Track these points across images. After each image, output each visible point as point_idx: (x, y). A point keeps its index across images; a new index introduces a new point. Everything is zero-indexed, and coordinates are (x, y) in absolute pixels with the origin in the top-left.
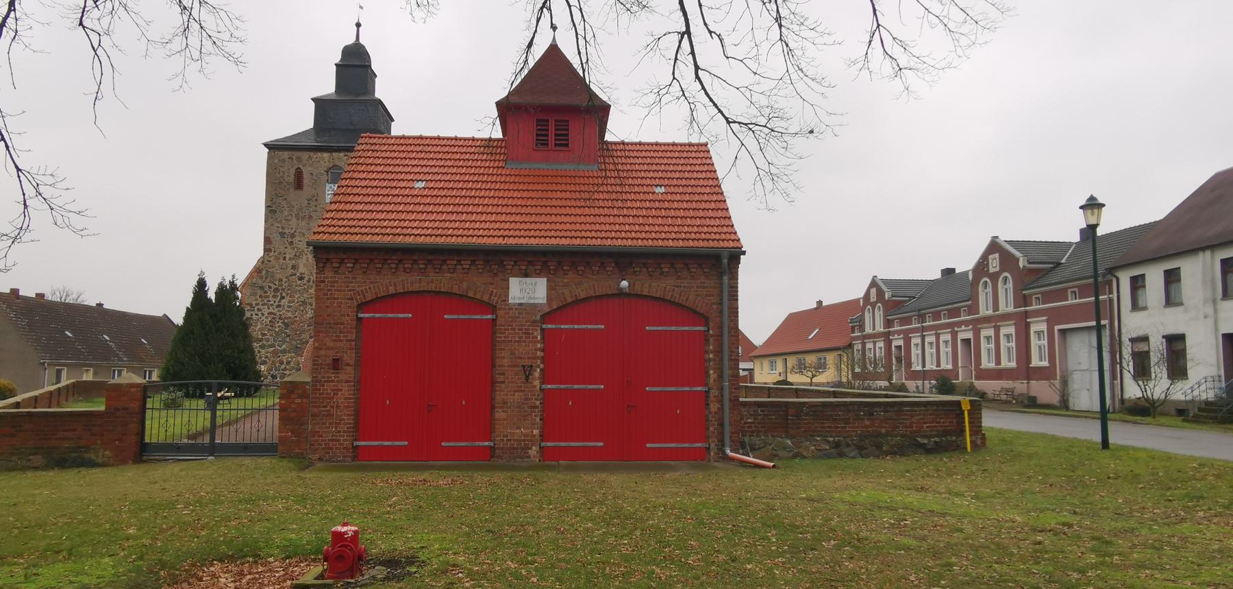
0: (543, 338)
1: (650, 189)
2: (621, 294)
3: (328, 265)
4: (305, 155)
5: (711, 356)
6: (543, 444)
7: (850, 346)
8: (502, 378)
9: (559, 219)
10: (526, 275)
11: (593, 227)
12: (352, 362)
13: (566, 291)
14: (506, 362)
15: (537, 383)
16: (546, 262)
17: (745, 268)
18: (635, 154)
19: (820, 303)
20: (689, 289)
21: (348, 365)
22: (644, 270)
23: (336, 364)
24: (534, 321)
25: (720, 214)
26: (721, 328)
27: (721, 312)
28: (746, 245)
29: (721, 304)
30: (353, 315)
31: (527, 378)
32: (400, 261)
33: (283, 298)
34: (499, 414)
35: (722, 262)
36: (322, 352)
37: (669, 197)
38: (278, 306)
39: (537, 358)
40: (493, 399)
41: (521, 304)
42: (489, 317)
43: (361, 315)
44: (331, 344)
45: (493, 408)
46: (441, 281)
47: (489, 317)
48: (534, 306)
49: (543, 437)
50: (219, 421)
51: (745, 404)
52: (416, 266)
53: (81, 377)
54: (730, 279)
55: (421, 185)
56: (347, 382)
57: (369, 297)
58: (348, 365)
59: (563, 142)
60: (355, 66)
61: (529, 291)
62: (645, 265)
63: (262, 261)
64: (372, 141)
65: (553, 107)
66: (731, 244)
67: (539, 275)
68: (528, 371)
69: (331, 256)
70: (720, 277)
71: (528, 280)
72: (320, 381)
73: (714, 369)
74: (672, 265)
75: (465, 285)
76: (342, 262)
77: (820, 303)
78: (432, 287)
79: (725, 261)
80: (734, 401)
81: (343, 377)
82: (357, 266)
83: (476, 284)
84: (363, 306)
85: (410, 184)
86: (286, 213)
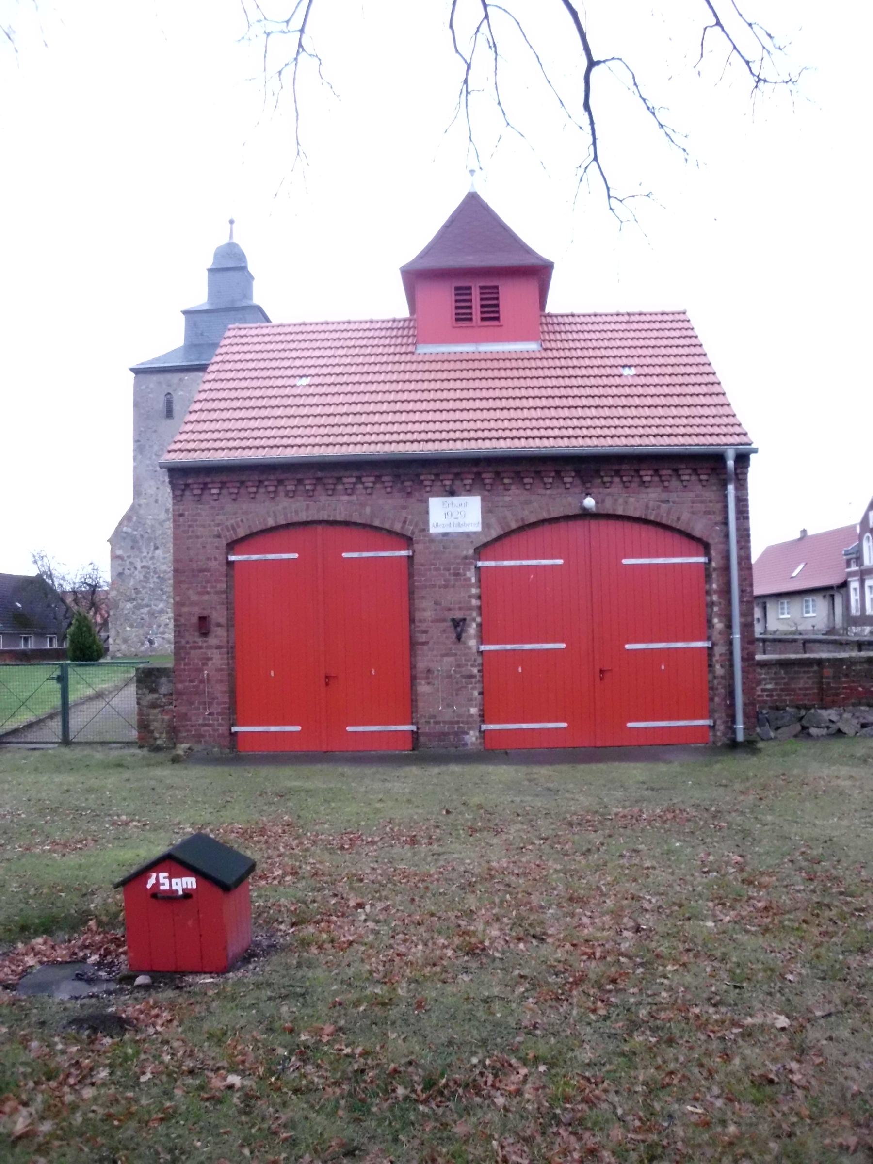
0: (479, 580)
1: (615, 371)
2: (586, 515)
3: (187, 493)
4: (175, 378)
5: (715, 598)
6: (484, 727)
7: (845, 585)
8: (423, 638)
9: (509, 383)
10: (452, 493)
11: (541, 423)
12: (223, 621)
13: (509, 514)
14: (428, 614)
15: (473, 643)
16: (478, 474)
17: (757, 473)
18: (590, 327)
19: (804, 532)
20: (683, 502)
21: (219, 625)
22: (617, 479)
23: (204, 625)
24: (466, 557)
25: (716, 400)
26: (727, 557)
27: (727, 536)
28: (756, 438)
29: (726, 523)
30: (221, 558)
31: (459, 638)
32: (280, 482)
33: (156, 548)
34: (423, 688)
35: (719, 468)
36: (185, 609)
37: (642, 380)
38: (152, 558)
39: (470, 608)
40: (413, 667)
41: (446, 534)
42: (404, 553)
43: (232, 558)
44: (195, 598)
45: (413, 678)
46: (338, 505)
47: (404, 553)
48: (468, 535)
49: (483, 718)
50: (72, 698)
51: (763, 664)
52: (301, 488)
53: (18, 645)
54: (736, 489)
55: (305, 381)
56: (218, 647)
57: (241, 533)
58: (219, 625)
59: (491, 313)
60: (230, 267)
61: (455, 515)
62: (618, 473)
63: (132, 508)
64: (243, 332)
65: (479, 277)
66: (736, 440)
67: (469, 492)
68: (459, 625)
69: (190, 481)
70: (724, 486)
71: (455, 500)
72: (184, 648)
73: (719, 616)
74: (656, 471)
75: (368, 510)
76: (205, 487)
77: (804, 532)
78: (324, 516)
79: (731, 463)
80: (748, 658)
81: (213, 641)
82: (224, 491)
83: (381, 505)
84: (233, 546)
85: (291, 382)
86: (156, 448)
